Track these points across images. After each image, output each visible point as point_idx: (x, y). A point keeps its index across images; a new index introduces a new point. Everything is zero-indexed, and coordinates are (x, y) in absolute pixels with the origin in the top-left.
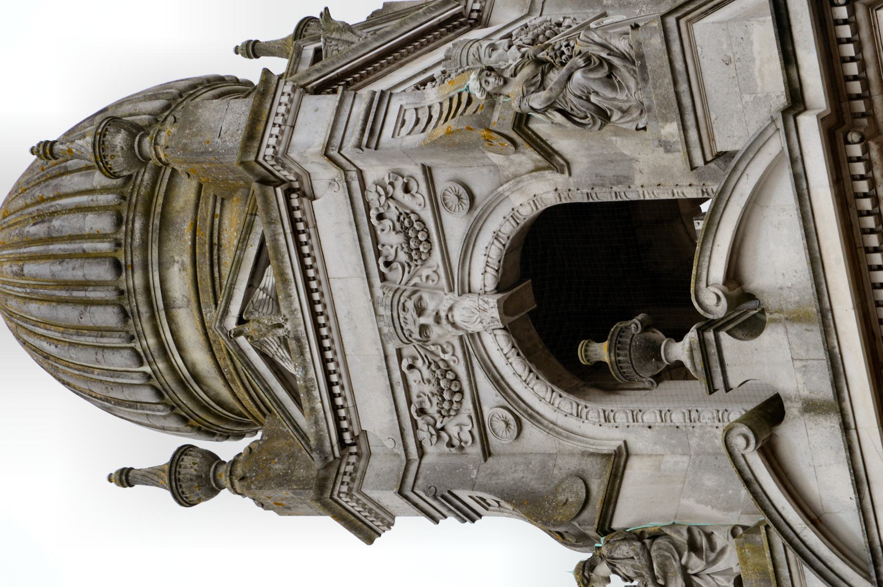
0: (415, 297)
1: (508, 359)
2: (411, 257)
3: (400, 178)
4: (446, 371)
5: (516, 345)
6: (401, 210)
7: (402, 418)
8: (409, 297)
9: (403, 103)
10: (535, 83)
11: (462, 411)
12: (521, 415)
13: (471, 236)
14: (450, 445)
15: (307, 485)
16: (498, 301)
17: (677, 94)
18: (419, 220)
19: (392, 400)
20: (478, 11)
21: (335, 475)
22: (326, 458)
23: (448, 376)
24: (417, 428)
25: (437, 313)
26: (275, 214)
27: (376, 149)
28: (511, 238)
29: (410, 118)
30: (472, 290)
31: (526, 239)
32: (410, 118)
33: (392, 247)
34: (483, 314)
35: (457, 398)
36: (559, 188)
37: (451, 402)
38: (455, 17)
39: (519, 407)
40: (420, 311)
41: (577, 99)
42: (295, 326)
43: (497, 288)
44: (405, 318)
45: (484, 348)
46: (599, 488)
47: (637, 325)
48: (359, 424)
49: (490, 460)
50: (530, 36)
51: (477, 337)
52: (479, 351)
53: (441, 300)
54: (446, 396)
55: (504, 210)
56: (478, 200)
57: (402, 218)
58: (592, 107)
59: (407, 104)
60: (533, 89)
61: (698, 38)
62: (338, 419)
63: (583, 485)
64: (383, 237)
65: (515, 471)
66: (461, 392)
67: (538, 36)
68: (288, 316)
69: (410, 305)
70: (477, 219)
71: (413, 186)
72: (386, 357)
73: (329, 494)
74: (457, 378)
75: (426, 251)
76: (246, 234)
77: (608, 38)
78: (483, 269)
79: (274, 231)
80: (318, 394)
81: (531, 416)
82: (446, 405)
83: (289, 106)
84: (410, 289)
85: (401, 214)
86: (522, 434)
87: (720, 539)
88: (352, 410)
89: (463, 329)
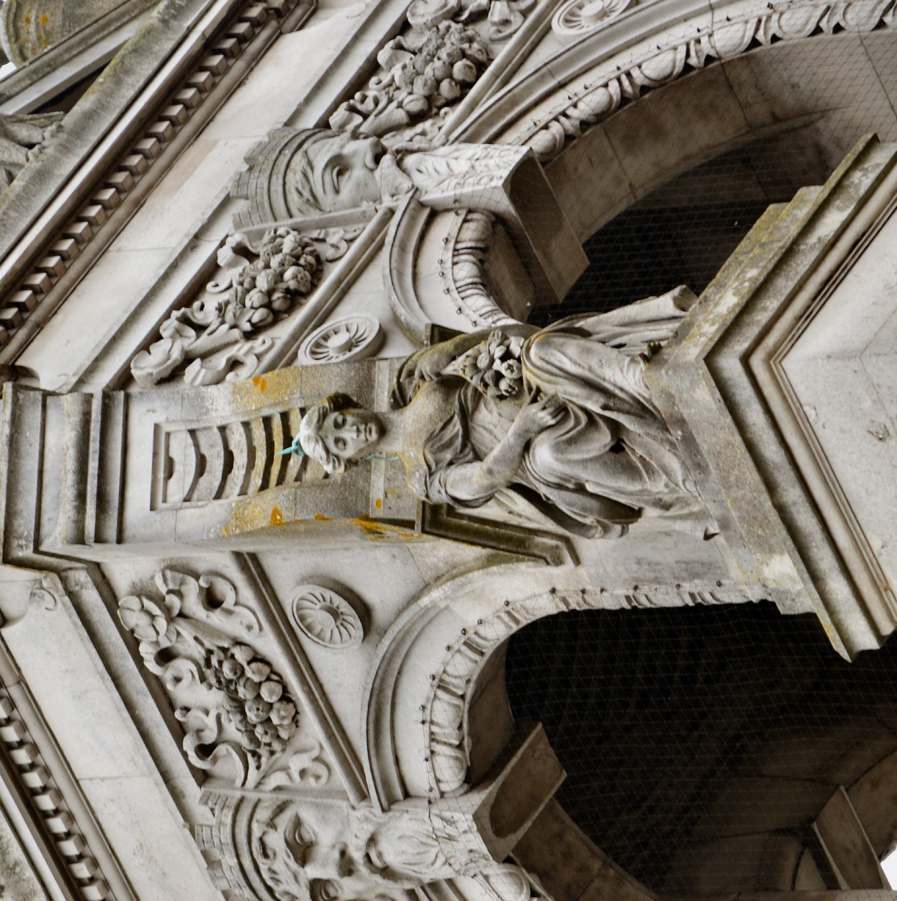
0: (285, 821)
2: (254, 739)
3: (191, 581)
5: (539, 889)
6: (208, 645)
8: (271, 824)
9: (160, 418)
10: (450, 443)
13: (381, 691)
16: (476, 817)
17: (782, 510)
18: (257, 658)
25: (343, 853)
27: (120, 540)
28: (474, 678)
31: (508, 665)
33: (207, 713)
34: (447, 847)
36: (559, 587)
40: (302, 851)
41: (556, 492)
43: (467, 780)
44: (272, 871)
50: (420, 89)
51: (445, 886)
53: (346, 822)
55: (444, 633)
56: (381, 614)
57: (214, 661)
58: (594, 504)
59: (167, 421)
60: (448, 455)
61: (800, 389)
64: (183, 694)
67: (438, 82)
69: (276, 840)
71: (223, 588)
75: (286, 722)
77: (594, 363)
78: (428, 743)
84: (269, 800)
85: (210, 652)
89: (409, 878)
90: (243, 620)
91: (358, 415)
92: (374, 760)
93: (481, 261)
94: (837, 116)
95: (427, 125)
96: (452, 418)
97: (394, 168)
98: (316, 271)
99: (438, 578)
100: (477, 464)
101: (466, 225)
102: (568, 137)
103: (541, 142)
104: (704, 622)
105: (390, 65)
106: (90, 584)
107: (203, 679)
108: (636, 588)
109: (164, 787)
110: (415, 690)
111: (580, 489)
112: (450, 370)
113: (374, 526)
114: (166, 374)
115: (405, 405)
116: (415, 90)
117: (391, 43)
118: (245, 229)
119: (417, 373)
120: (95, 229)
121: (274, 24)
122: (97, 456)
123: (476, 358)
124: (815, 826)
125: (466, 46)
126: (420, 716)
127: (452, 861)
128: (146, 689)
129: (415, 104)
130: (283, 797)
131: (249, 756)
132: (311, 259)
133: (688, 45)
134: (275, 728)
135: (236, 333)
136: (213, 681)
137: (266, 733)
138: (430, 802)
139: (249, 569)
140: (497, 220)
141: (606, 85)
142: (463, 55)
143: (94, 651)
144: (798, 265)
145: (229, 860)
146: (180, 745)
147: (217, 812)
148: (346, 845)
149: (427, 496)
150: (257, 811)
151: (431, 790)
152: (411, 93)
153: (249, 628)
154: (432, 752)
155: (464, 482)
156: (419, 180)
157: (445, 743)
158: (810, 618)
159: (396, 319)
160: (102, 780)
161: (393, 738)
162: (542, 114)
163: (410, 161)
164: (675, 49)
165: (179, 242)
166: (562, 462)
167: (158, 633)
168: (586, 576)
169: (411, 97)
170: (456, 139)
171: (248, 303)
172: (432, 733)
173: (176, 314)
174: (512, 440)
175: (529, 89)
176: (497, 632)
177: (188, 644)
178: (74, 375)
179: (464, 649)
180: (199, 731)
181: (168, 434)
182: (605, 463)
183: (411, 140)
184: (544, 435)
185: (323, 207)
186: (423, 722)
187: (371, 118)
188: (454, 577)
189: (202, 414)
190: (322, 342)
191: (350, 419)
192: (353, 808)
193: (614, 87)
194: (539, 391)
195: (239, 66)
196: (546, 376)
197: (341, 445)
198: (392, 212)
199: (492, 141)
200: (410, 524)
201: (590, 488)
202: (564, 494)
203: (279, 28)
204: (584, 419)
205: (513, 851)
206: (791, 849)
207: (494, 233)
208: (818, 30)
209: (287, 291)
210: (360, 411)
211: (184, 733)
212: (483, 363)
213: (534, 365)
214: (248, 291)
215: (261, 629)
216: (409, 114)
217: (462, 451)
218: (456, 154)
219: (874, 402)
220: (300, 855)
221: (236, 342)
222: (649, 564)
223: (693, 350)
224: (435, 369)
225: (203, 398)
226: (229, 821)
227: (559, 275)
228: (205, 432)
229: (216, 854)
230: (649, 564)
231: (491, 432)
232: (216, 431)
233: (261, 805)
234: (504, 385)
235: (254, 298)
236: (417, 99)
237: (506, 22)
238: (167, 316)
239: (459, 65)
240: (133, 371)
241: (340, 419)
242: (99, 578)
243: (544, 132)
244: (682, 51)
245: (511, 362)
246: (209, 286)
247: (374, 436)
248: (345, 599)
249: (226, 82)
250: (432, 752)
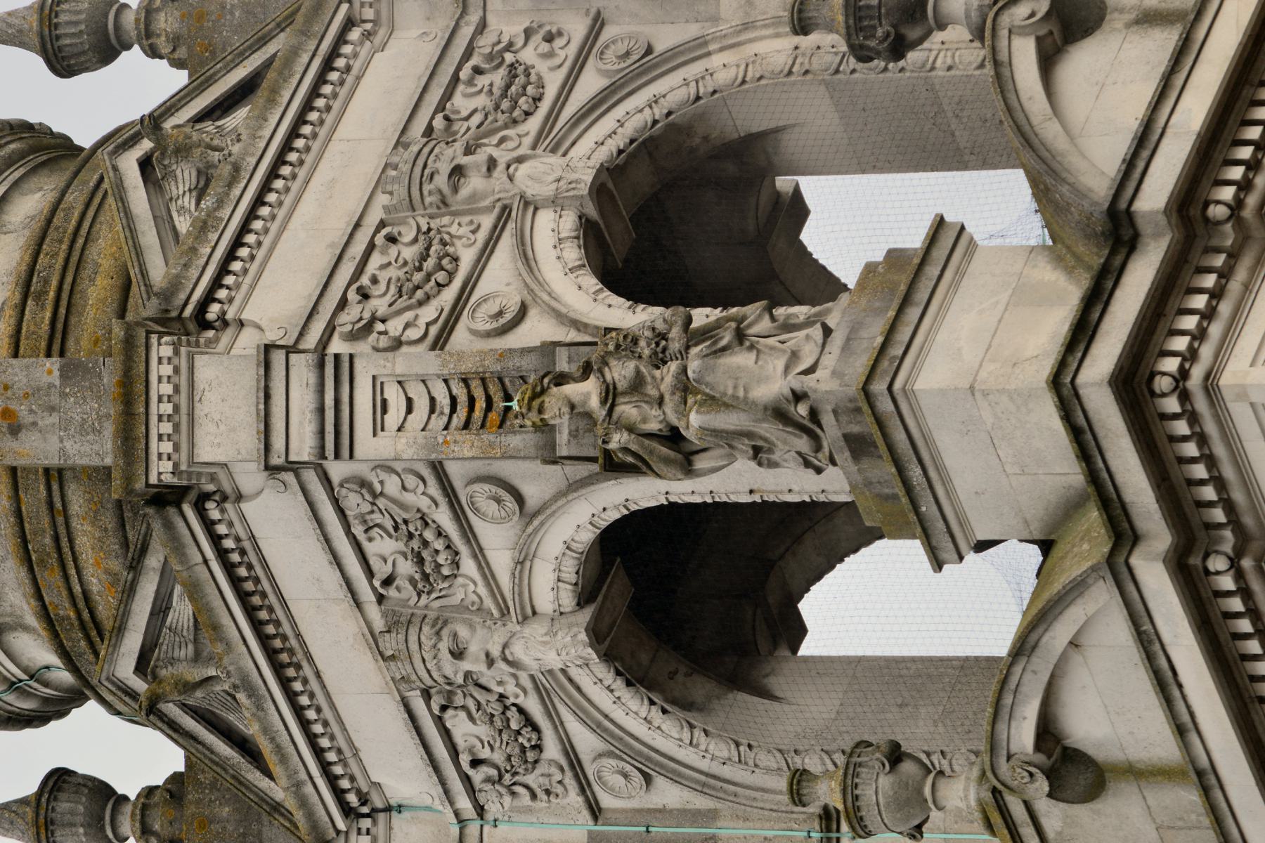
7: (443, 66)
19: (328, 272)
26: (317, 28)
30: (538, 609)
37: (428, 277)
42: (245, 153)
43: (578, 604)
54: (429, 264)
68: (243, 137)
72: (357, 225)
76: (250, 47)
78: (551, 583)
79: (301, 44)
82: (418, 277)
83: (233, 293)
164: (738, 66)
244: (743, 67)
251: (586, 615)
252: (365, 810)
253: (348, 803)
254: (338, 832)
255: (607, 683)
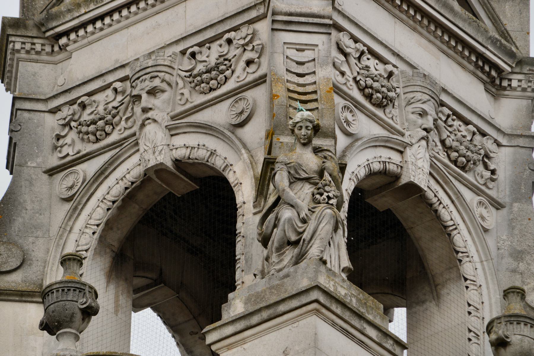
0: (164, 86)
1: (122, 179)
2: (195, 76)
3: (257, 55)
4: (112, 124)
5: (134, 185)
6: (232, 60)
8: (163, 81)
9: (320, 47)
10: (297, 173)
11: (85, 144)
12: (75, 201)
13: (211, 129)
14: (58, 137)
15: (27, 10)
16: (162, 164)
17: (259, 310)
20: (510, 85)
21: (30, 35)
22: (43, 25)
23: (107, 126)
24: (71, 105)
25: (151, 109)
29: (307, 55)
30: (173, 137)
32: (307, 55)
33: (207, 57)
34: (150, 151)
35: (92, 138)
36: (246, 205)
38: (494, 66)
39: (82, 197)
40: (152, 92)
43: (176, 160)
45: (129, 157)
46: (12, 282)
47: (85, 303)
48: (76, 50)
49: (46, 176)
50: (455, 144)
51: (137, 148)
52: (126, 152)
53: (162, 111)
54: (92, 128)
55: (231, 158)
56: (240, 132)
57: (226, 62)
59: (319, 50)
60: (292, 172)
62: (75, 29)
63: (19, 264)
64: (215, 46)
65: (33, 202)
66: (98, 140)
67: (457, 151)
69: (157, 82)
70: (223, 134)
71: (253, 68)
73: (11, 33)
74: (107, 134)
78: (190, 145)
80: (91, 9)
81: (75, 208)
84: (172, 79)
85: (230, 61)
86: (65, 202)
87: (494, 336)
88: (86, 41)
89: (140, 134)
90: (241, 75)
91: (311, 135)
92: (185, 124)
93: (380, 172)
94: (437, 308)
95: (440, 146)
96: (307, 174)
97: (421, 136)
98: (379, 105)
99: (252, 156)
100: (288, 184)
101: (395, 166)
102: (431, 205)
103: (430, 195)
104: (230, 262)
105: (468, 130)
106: (258, 14)
107: (220, 56)
108: (243, 237)
109: (180, 37)
110: (211, 143)
111: (275, 226)
112: (326, 174)
113: (270, 135)
114: (340, 46)
115: (314, 153)
116: (454, 142)
117: (476, 130)
118: (400, 75)
119: (325, 160)
120: (404, 13)
121: (488, 80)
122: (307, 21)
123: (329, 186)
124: (162, 285)
125: (472, 162)
126: (201, 144)
127: (146, 152)
128: (218, 33)
129: (448, 142)
130: (174, 85)
131: (190, 73)
132: (385, 103)
133: (466, 252)
134: (200, 85)
135: (355, 74)
136: (219, 61)
137: (198, 81)
138: (168, 145)
139: (260, 79)
140: (397, 177)
141: (452, 219)
142: (468, 161)
143: (233, 13)
144: (355, 320)
145: (150, 63)
146: (196, 45)
147: (169, 58)
148: (154, 110)
149: (277, 162)
150: (169, 75)
151: (173, 146)
152: (453, 140)
153: (238, 77)
154: (187, 147)
155: (282, 178)
156: (416, 146)
157: (190, 153)
158: (219, 318)
159: (357, 140)
160: (185, 12)
161: (193, 132)
162: (441, 194)
163: (424, 143)
164: (465, 247)
165: (397, 48)
166: (284, 221)
167: (238, 40)
168: (249, 217)
169: (451, 140)
170: (432, 161)
171: (367, 79)
172: (194, 148)
173: (365, 49)
174: (295, 200)
175: (451, 189)
176: (231, 178)
177: (234, 52)
178: (342, 9)
179: (225, 164)
180: (201, 53)
181: (314, 50)
182: (283, 238)
183: (433, 141)
184: (296, 214)
185: (407, 107)
186: (199, 145)
187: (444, 125)
188: (251, 163)
189: (320, 65)
190: (350, 110)
191: (309, 132)
192: (168, 114)
193: (451, 223)
194: (313, 212)
195: (472, 67)
196: (319, 216)
197: (299, 128)
198: (403, 135)
199: (430, 174)
200: (269, 153)
201: (275, 230)
202: (274, 219)
203: (487, 82)
204: (301, 230)
205: (148, 176)
206: (154, 276)
207: (392, 177)
208: (469, 305)
209: (372, 94)
210: (313, 136)
211: (200, 47)
212: (327, 188)
213: (323, 211)
214: (373, 79)
215: (238, 82)
216: (445, 140)
217: (294, 177)
218: (425, 161)
219: (298, 351)
220: (151, 92)
221: (352, 74)
222: (252, 243)
223: (323, 281)
224: (326, 168)
225: (327, 65)
226: (166, 63)
227: (376, 200)
228: (313, 66)
229: (153, 57)
230: (252, 243)
231: (301, 189)
232: (314, 70)
233: (171, 76)
234: (318, 196)
235: (369, 81)
236: (450, 143)
237: (482, 177)
238: (365, 45)
239: (464, 159)
240: (342, 33)
241: (309, 128)
242: (261, 17)
243: (433, 195)
244: (464, 250)
245: (327, 200)
246: (377, 61)
247: (303, 141)
248: (246, 118)
249: (465, 63)
250: (187, 147)
251: (169, 164)
252: (56, 48)
253: (61, 38)
254: (44, 32)
255: (127, 176)
